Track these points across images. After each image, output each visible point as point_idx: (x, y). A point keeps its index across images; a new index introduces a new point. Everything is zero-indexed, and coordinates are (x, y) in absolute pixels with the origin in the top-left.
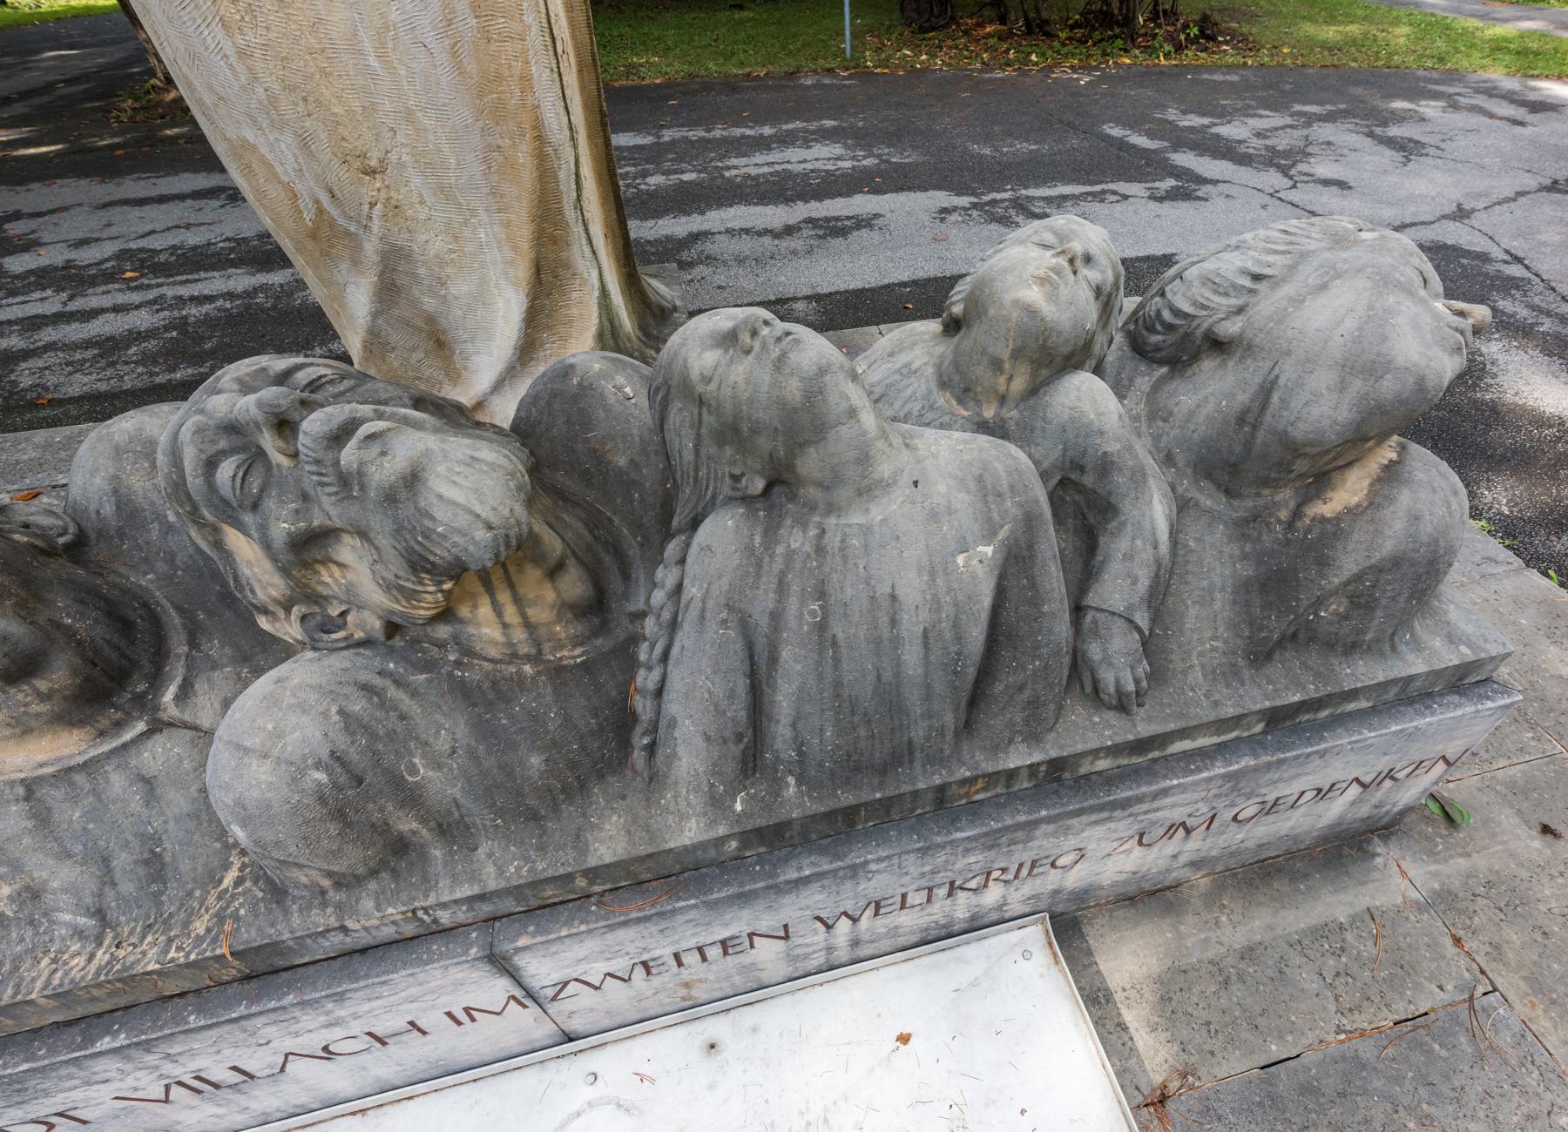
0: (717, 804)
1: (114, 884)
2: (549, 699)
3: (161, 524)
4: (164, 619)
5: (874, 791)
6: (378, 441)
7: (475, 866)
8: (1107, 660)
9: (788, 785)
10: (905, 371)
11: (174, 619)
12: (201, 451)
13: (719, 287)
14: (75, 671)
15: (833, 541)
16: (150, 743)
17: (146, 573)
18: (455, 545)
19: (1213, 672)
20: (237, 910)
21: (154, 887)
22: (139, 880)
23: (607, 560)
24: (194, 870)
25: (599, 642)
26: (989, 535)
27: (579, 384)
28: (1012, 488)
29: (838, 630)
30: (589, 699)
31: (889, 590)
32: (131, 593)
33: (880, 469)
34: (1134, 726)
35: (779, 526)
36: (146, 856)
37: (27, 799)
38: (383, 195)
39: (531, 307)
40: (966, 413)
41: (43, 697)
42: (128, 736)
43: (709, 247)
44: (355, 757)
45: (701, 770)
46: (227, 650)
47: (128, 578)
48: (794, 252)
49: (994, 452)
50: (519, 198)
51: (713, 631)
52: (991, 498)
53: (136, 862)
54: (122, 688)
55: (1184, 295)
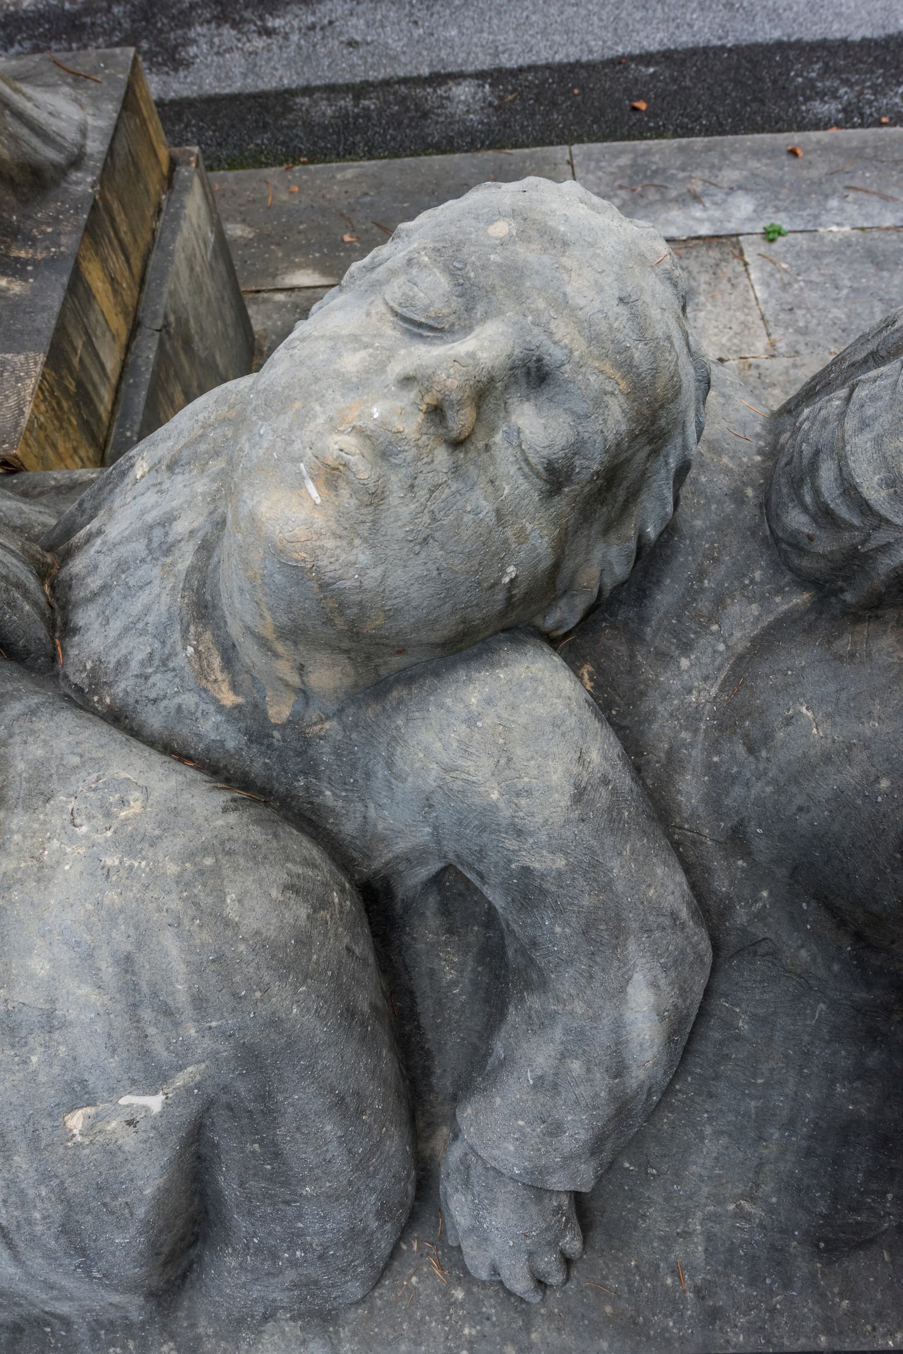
19: (732, 1250)
28: (199, 1002)
33: (528, 408)
34: (527, 1328)
55: (878, 441)
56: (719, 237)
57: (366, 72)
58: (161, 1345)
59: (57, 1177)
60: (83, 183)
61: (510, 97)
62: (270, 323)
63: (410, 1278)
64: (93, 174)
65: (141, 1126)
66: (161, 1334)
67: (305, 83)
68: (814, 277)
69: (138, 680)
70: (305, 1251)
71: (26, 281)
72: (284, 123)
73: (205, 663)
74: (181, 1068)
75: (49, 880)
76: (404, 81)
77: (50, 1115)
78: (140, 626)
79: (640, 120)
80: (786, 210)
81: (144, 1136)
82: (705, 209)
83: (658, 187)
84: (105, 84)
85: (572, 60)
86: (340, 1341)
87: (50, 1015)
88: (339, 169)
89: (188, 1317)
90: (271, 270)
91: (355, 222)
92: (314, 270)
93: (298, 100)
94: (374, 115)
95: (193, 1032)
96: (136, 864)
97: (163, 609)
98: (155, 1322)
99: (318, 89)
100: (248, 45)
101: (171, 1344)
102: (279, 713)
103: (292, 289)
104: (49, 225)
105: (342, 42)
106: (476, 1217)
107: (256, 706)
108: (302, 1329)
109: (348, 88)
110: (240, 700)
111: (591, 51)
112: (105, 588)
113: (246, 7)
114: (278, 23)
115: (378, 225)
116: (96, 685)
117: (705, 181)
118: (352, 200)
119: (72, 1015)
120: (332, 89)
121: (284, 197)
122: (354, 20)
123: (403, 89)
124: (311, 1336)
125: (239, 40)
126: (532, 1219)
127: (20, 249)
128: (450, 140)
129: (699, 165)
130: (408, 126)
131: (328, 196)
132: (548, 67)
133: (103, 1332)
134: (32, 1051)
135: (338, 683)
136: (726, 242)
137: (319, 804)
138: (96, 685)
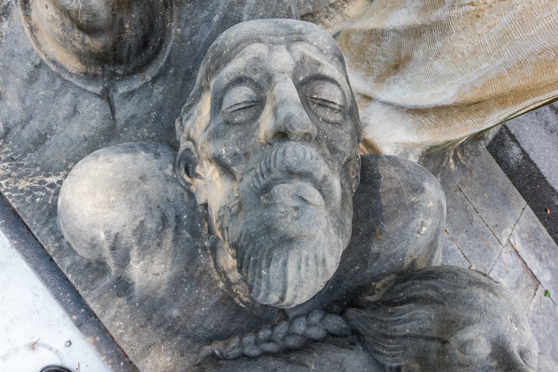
1: (23, 127)
2: (211, 303)
3: (209, 15)
4: (160, 56)
6: (303, 203)
7: (111, 303)
11: (161, 62)
12: (245, 69)
14: (104, 47)
16: (94, 99)
17: (179, 27)
18: (259, 284)
20: (38, 197)
21: (31, 146)
22: (31, 137)
24: (48, 159)
30: (222, 320)
32: (165, 33)
36: (43, 133)
37: (36, 67)
38: (482, 7)
39: (448, 107)
41: (83, 43)
42: (90, 88)
44: (123, 242)
46: (161, 97)
47: (172, 21)
48: (547, 123)
50: (525, 78)
53: (38, 131)
54: (114, 65)
56: (536, 277)
61: (524, 167)
68: (546, 319)
79: (545, 215)
80: (555, 290)
82: (540, 265)
83: (536, 245)
85: (545, 175)
111: (550, 179)
117: (546, 257)
128: (502, 161)
129: (548, 250)
132: (538, 170)
135: (275, 92)
136: (537, 282)
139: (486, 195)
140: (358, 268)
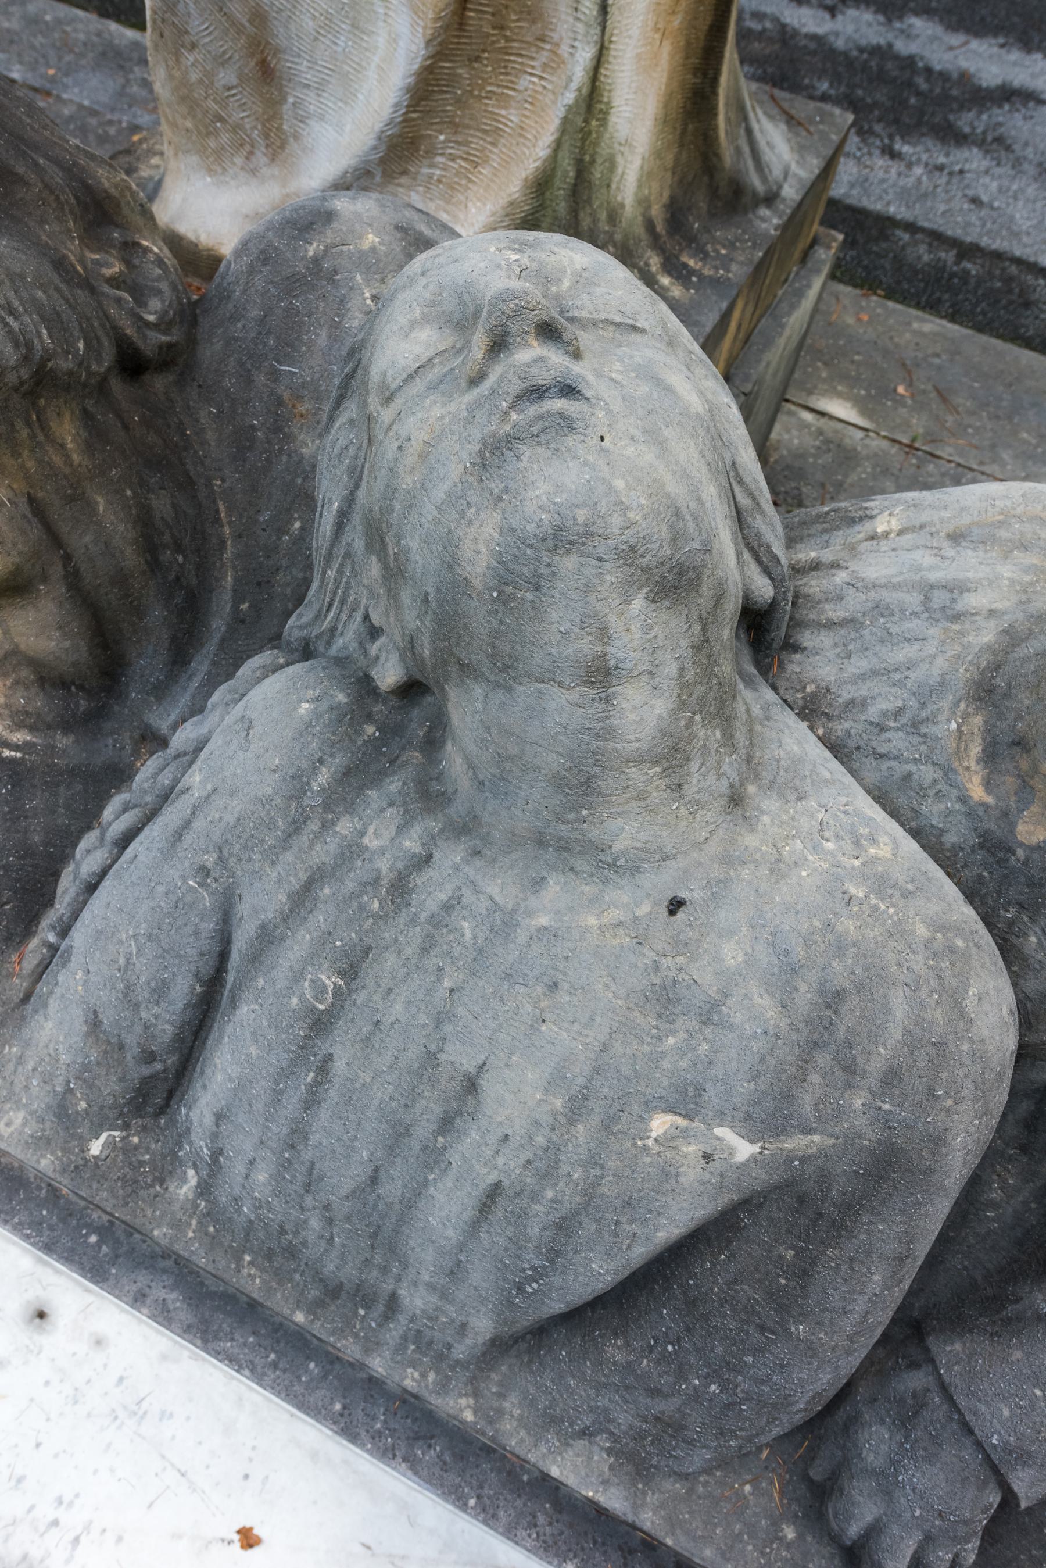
0: (65, 1121)
5: (298, 1305)
8: (887, 1486)
9: (184, 1180)
10: (939, 598)
13: (975, 201)
15: (432, 891)
23: (157, 613)
25: (63, 741)
26: (768, 1120)
27: (316, 261)
28: (892, 1077)
29: (341, 1050)
31: (469, 1066)
35: (378, 779)
40: (977, 792)
43: (1015, 123)
45: (65, 1058)
49: (919, 963)
51: (178, 873)
52: (823, 1059)
57: (981, 235)
58: (461, 1396)
59: (602, 1167)
60: (769, 222)
62: (786, 437)
63: (744, 1484)
64: (780, 217)
65: (716, 1166)
66: (466, 1385)
67: (911, 219)
69: (870, 728)
70: (723, 1389)
71: (688, 290)
72: (875, 248)
73: (963, 745)
74: (806, 1131)
75: (782, 877)
76: (1019, 261)
77: (646, 1103)
78: (897, 676)
81: (707, 1176)
84: (816, 137)
86: (644, 1504)
87: (715, 1006)
88: (917, 318)
89: (500, 1384)
90: (809, 386)
91: (915, 378)
92: (854, 406)
93: (899, 233)
94: (973, 281)
95: (858, 1103)
96: (883, 907)
97: (936, 672)
98: (467, 1369)
99: (922, 230)
100: (866, 157)
101: (471, 1401)
102: (1030, 833)
103: (822, 414)
104: (724, 247)
105: (965, 196)
106: (893, 1462)
107: (1005, 814)
108: (611, 1468)
109: (954, 243)
110: (990, 800)
112: (848, 622)
113: (879, 120)
114: (906, 149)
115: (938, 391)
116: (811, 710)
118: (920, 355)
119: (737, 1019)
120: (937, 237)
121: (850, 320)
122: (987, 180)
123: (1013, 269)
124: (616, 1481)
125: (859, 149)
126: (962, 1501)
127: (691, 257)
130: (1005, 308)
131: (896, 340)
133: (413, 1347)
134: (673, 1032)
137: (1013, 946)
138: (811, 710)
139: (1025, 435)
140: (297, 525)
